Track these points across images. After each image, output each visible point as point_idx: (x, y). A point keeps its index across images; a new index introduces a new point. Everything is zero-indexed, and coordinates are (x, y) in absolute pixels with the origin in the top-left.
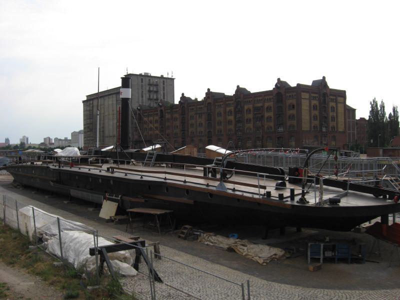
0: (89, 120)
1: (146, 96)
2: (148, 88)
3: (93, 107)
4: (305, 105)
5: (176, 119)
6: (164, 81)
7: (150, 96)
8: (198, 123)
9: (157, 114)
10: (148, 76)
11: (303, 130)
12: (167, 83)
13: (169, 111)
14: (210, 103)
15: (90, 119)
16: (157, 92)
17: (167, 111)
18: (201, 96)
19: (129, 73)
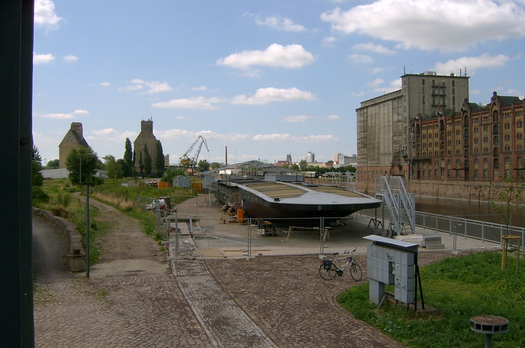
0: (363, 134)
1: (429, 101)
2: (431, 92)
3: (367, 117)
4: (324, 238)
5: (458, 132)
6: (453, 82)
7: (434, 102)
8: (483, 137)
9: (437, 125)
10: (432, 76)
11: (351, 149)
12: (113, 158)
13: (451, 121)
14: (496, 111)
15: (364, 131)
16: (443, 96)
17: (448, 122)
18: (158, 139)
19: (406, 74)
